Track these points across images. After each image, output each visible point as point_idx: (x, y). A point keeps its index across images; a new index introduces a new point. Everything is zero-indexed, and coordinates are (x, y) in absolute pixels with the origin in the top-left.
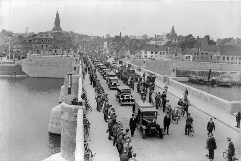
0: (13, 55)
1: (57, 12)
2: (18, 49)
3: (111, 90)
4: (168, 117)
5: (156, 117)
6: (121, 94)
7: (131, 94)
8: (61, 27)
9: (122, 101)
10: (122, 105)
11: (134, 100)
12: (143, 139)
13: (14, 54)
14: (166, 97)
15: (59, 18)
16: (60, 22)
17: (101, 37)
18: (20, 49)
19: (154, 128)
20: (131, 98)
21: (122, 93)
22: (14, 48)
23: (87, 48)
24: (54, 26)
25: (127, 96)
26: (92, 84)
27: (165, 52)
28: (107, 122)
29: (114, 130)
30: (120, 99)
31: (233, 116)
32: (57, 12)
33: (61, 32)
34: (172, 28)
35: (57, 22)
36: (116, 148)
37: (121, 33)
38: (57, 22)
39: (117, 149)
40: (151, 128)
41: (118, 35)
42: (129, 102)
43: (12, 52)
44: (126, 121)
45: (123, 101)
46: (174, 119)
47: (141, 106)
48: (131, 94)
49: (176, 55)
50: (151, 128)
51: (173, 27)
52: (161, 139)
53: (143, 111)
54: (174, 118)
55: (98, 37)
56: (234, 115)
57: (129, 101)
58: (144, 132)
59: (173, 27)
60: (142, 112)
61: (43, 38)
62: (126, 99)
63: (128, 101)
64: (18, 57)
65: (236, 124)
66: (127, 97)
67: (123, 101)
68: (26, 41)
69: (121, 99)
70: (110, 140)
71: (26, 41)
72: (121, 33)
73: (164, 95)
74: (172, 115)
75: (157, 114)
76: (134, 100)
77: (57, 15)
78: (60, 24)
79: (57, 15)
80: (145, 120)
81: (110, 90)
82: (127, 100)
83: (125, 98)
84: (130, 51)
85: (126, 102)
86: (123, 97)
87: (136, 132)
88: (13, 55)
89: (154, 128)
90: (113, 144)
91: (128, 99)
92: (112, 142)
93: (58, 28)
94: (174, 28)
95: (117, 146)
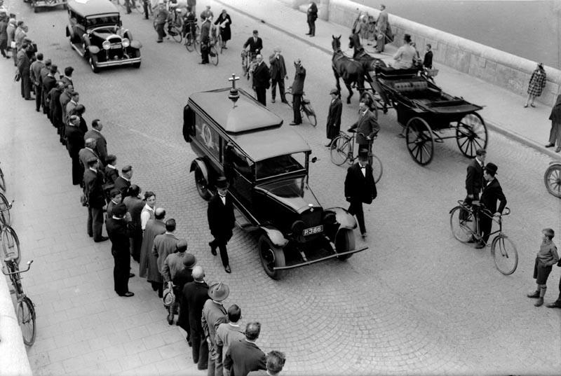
3: (36, 12)
4: (364, 171)
5: (306, 172)
6: (89, 31)
7: (122, 28)
9: (95, 58)
10: (98, 71)
11: (138, 50)
12: (96, 75)
14: (262, 47)
19: (317, 230)
20: (126, 44)
21: (91, 28)
25: (113, 36)
26: (41, 109)
28: (8, 57)
29: (33, 74)
30: (88, 50)
31: (300, 13)
36: (46, 116)
39: (49, 117)
40: (306, 232)
42: (120, 58)
44: (58, 49)
45: (102, 56)
46: (172, 33)
47: (234, 130)
48: (124, 29)
50: (306, 232)
52: (138, 70)
53: (256, 160)
54: (172, 30)
56: (302, 11)
57: (121, 56)
58: (280, 257)
60: (250, 164)
62: (110, 49)
63: (120, 53)
65: (307, 29)
66: (113, 41)
67: (102, 56)
69: (94, 49)
70: (27, 99)
73: (255, 39)
74: (166, 25)
75: (311, 157)
76: (138, 50)
80: (269, 193)
81: (35, 14)
82: (112, 54)
83: (107, 46)
85: (112, 58)
86: (97, 41)
87: (236, 246)
89: (317, 230)
90: (35, 107)
91: (117, 46)
92: (33, 104)
95: (46, 111)
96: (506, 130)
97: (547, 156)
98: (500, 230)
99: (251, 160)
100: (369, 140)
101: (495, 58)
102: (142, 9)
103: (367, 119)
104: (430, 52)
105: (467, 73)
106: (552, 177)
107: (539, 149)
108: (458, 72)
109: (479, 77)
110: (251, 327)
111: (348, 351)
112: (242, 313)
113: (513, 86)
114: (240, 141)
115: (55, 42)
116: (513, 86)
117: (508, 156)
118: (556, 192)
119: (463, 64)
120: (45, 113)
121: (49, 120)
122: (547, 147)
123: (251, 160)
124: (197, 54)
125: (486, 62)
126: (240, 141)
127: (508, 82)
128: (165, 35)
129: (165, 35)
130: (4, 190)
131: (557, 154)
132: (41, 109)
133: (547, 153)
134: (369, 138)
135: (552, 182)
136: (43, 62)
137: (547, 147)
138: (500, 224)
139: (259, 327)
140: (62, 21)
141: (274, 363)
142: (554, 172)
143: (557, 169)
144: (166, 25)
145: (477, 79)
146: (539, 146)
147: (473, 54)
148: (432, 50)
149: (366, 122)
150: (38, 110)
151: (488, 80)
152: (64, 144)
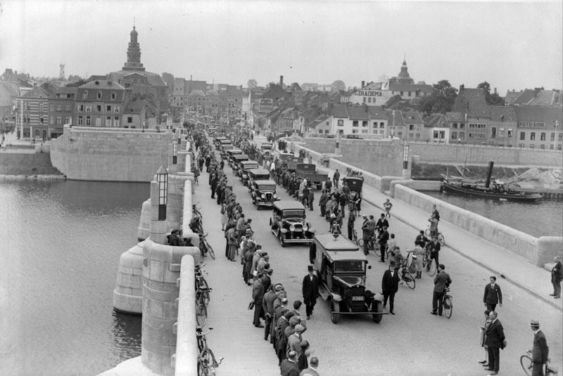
0: (31, 128)
1: (134, 28)
2: (43, 113)
3: (258, 209)
4: (392, 274)
5: (364, 274)
6: (283, 220)
7: (306, 220)
8: (141, 62)
9: (284, 236)
10: (285, 245)
11: (313, 234)
12: (335, 325)
13: (32, 126)
15: (138, 42)
16: (141, 51)
17: (236, 87)
18: (46, 114)
19: (361, 298)
20: (305, 229)
21: (285, 218)
22: (32, 113)
24: (126, 62)
25: (298, 223)
26: (216, 196)
27: (386, 122)
28: (249, 284)
29: (266, 304)
30: (280, 231)
31: (545, 271)
32: (134, 28)
33: (141, 74)
34: (401, 65)
35: (134, 51)
36: (272, 345)
37: (282, 77)
38: (134, 51)
39: (274, 347)
40: (354, 298)
41: (277, 81)
42: (301, 238)
43: (29, 122)
44: (294, 281)
45: (288, 235)
46: (406, 278)
47: (329, 248)
48: (307, 220)
49: (411, 127)
50: (354, 298)
51: (405, 64)
52: (377, 325)
53: (334, 260)
54: (406, 275)
55: (228, 86)
56: (547, 270)
57: (301, 237)
58: (337, 307)
59: (405, 64)
60: (331, 262)
61: (101, 90)
62: (294, 232)
63: (300, 235)
64: (41, 133)
65: (552, 290)
66: (297, 226)
67: (288, 235)
68: (61, 96)
69: (284, 230)
70: (257, 326)
71: (61, 96)
72: (282, 77)
74: (401, 270)
75: (368, 265)
76: (313, 234)
77: (134, 35)
78: (141, 55)
79: (134, 35)
80: (340, 280)
81: (257, 211)
82: (296, 235)
83: (292, 229)
84: (303, 118)
85: (295, 237)
86: (287, 226)
87: (319, 308)
88: (31, 128)
89: (361, 298)
90: (264, 336)
91: (299, 230)
92: (262, 331)
93: (134, 65)
94: (407, 66)
95: (274, 341)
125: (204, 113)
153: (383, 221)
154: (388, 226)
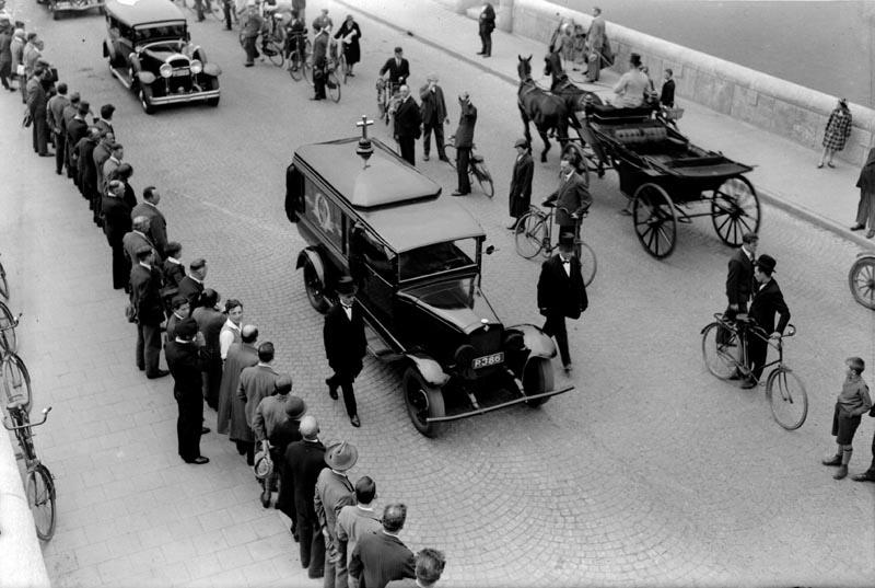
3: (56, 18)
4: (567, 267)
5: (477, 270)
6: (139, 49)
7: (191, 44)
9: (149, 91)
10: (153, 110)
11: (215, 78)
12: (150, 117)
19: (494, 359)
20: (196, 69)
21: (142, 44)
23: (758, 98)
25: (177, 56)
26: (64, 170)
28: (13, 90)
29: (52, 115)
30: (137, 79)
31: (468, 20)
36: (72, 181)
39: (76, 183)
40: (477, 363)
42: (187, 91)
44: (90, 77)
45: (159, 87)
46: (269, 51)
47: (365, 203)
48: (193, 46)
50: (477, 363)
52: (215, 110)
53: (399, 250)
54: (269, 47)
56: (471, 18)
57: (189, 88)
58: (437, 401)
60: (391, 256)
62: (171, 77)
63: (187, 83)
65: (479, 46)
66: (176, 64)
67: (159, 87)
69: (146, 77)
70: (42, 155)
74: (259, 40)
75: (485, 245)
76: (215, 78)
80: (420, 302)
81: (55, 22)
82: (175, 84)
83: (167, 73)
85: (175, 91)
86: (152, 65)
87: (368, 385)
89: (494, 359)
90: (55, 167)
91: (183, 73)
92: (52, 162)
95: (72, 174)
96: (789, 204)
97: (854, 244)
98: (780, 360)
99: (391, 251)
100: (575, 219)
101: (772, 91)
102: (221, 15)
103: (572, 186)
104: (671, 81)
105: (729, 113)
106: (860, 277)
107: (840, 234)
108: (714, 112)
109: (747, 120)
110: (391, 511)
111: (542, 548)
112: (377, 489)
113: (800, 134)
114: (374, 220)
115: (85, 66)
116: (800, 134)
117: (792, 244)
118: (868, 300)
119: (722, 101)
120: (70, 176)
121: (76, 188)
122: (853, 229)
123: (391, 251)
124: (308, 85)
126: (374, 220)
127: (792, 128)
128: (257, 55)
129: (257, 55)
130: (7, 298)
131: (869, 240)
132: (64, 170)
133: (853, 239)
134: (575, 215)
135: (860, 284)
136: (68, 96)
137: (853, 229)
138: (780, 350)
139: (405, 511)
140: (97, 32)
141: (427, 567)
142: (864, 270)
143: (869, 264)
144: (259, 40)
145: (745, 124)
146: (840, 228)
147: (738, 84)
148: (673, 78)
149: (570, 190)
150: (59, 172)
151: (761, 126)
152: (99, 225)
153: (398, 62)
154: (408, 74)
